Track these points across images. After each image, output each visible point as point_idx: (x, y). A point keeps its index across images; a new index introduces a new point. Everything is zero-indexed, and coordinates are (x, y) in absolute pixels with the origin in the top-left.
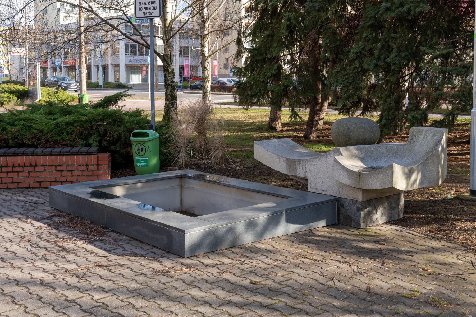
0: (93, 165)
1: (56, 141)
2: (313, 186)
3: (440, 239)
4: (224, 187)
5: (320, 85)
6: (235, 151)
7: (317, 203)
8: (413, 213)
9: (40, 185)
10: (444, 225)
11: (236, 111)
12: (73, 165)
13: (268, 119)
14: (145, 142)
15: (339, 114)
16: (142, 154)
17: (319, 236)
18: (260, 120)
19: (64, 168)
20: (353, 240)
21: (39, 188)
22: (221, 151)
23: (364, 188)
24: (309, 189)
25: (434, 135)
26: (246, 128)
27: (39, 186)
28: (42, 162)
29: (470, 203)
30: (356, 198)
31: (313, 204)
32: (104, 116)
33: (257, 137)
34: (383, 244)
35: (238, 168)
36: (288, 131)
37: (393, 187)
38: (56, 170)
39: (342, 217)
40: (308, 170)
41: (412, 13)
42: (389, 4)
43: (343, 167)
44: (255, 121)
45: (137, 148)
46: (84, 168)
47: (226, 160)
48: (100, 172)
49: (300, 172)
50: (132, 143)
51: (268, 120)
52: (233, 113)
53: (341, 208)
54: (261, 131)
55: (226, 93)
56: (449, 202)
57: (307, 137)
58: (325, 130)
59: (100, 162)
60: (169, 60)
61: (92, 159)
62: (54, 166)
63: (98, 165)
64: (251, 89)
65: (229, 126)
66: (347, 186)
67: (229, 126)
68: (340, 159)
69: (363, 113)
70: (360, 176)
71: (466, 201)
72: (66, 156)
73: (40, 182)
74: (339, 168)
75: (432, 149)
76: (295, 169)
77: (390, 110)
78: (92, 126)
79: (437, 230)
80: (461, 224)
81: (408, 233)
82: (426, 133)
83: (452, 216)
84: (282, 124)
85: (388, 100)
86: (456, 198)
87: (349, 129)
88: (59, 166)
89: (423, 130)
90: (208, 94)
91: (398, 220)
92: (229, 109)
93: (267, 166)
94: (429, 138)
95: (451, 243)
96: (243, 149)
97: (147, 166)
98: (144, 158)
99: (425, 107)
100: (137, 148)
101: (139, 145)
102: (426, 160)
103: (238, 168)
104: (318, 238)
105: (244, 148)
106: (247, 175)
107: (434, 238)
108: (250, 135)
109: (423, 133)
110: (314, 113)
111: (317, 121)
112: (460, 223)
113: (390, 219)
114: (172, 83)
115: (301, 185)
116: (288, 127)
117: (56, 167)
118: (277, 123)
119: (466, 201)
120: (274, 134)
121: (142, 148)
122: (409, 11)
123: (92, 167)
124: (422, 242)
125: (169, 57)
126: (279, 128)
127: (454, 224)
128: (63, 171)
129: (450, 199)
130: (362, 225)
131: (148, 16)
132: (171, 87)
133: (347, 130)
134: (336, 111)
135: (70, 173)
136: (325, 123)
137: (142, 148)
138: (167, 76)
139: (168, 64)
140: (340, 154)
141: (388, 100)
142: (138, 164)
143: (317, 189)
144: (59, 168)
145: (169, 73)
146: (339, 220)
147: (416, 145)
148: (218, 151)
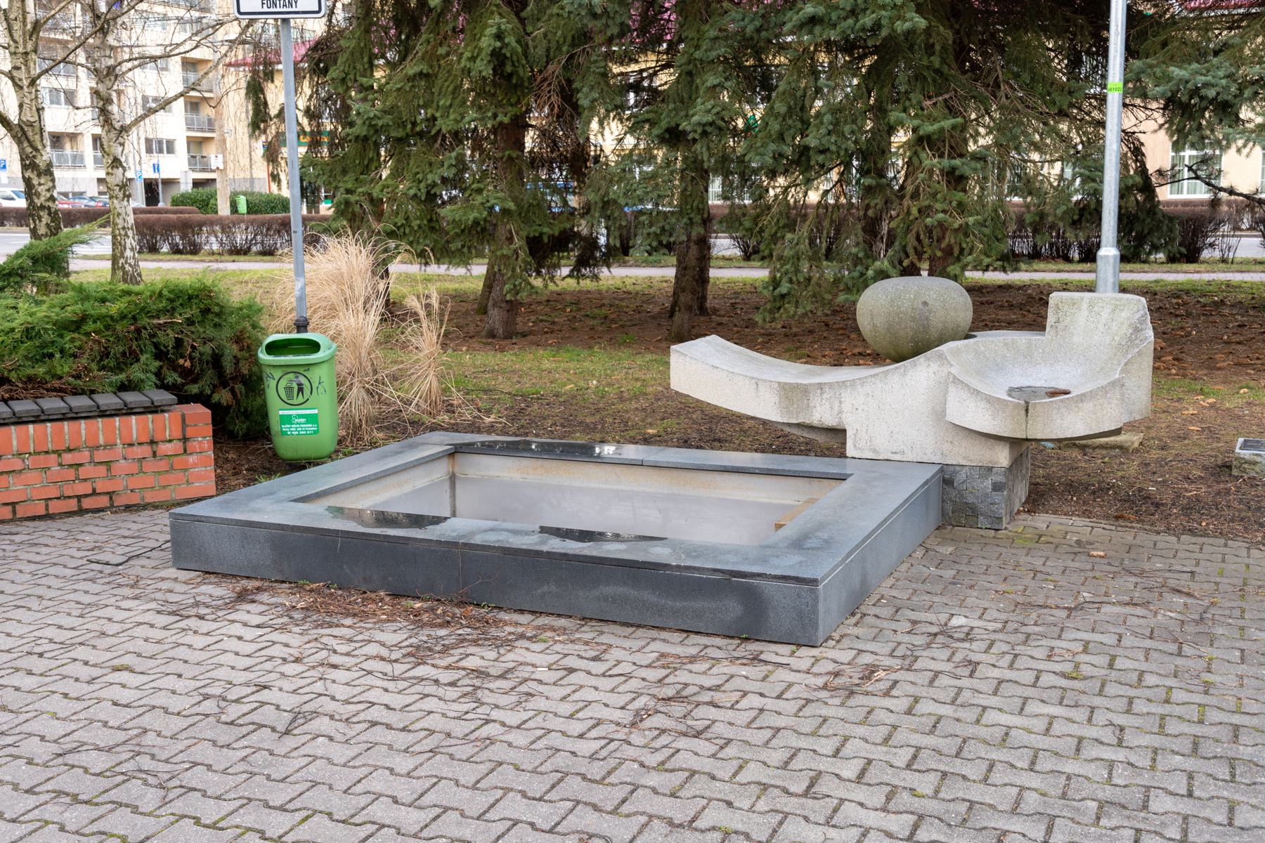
0: (170, 441)
1: (30, 379)
4: (609, 468)
9: (14, 512)
12: (110, 446)
14: (308, 366)
16: (301, 399)
19: (84, 457)
21: (12, 520)
24: (850, 451)
27: (10, 516)
28: (15, 443)
32: (171, 301)
38: (60, 465)
40: (847, 406)
41: (884, 33)
42: (821, 10)
45: (283, 383)
46: (146, 451)
48: (192, 459)
49: (822, 413)
50: (268, 371)
59: (190, 432)
60: (37, 137)
61: (168, 423)
62: (54, 452)
63: (185, 439)
69: (576, 273)
70: (1027, 410)
72: (89, 421)
73: (13, 504)
78: (138, 331)
87: (925, 303)
88: (69, 450)
97: (315, 432)
98: (308, 412)
100: (283, 383)
101: (291, 376)
109: (1085, 306)
114: (50, 204)
117: (60, 455)
121: (300, 385)
122: (877, 26)
123: (169, 445)
125: (37, 130)
128: (81, 465)
131: (278, 10)
132: (49, 214)
135: (103, 469)
137: (300, 385)
138: (35, 182)
139: (37, 150)
142: (285, 428)
143: (874, 451)
144: (68, 458)
145: (39, 175)
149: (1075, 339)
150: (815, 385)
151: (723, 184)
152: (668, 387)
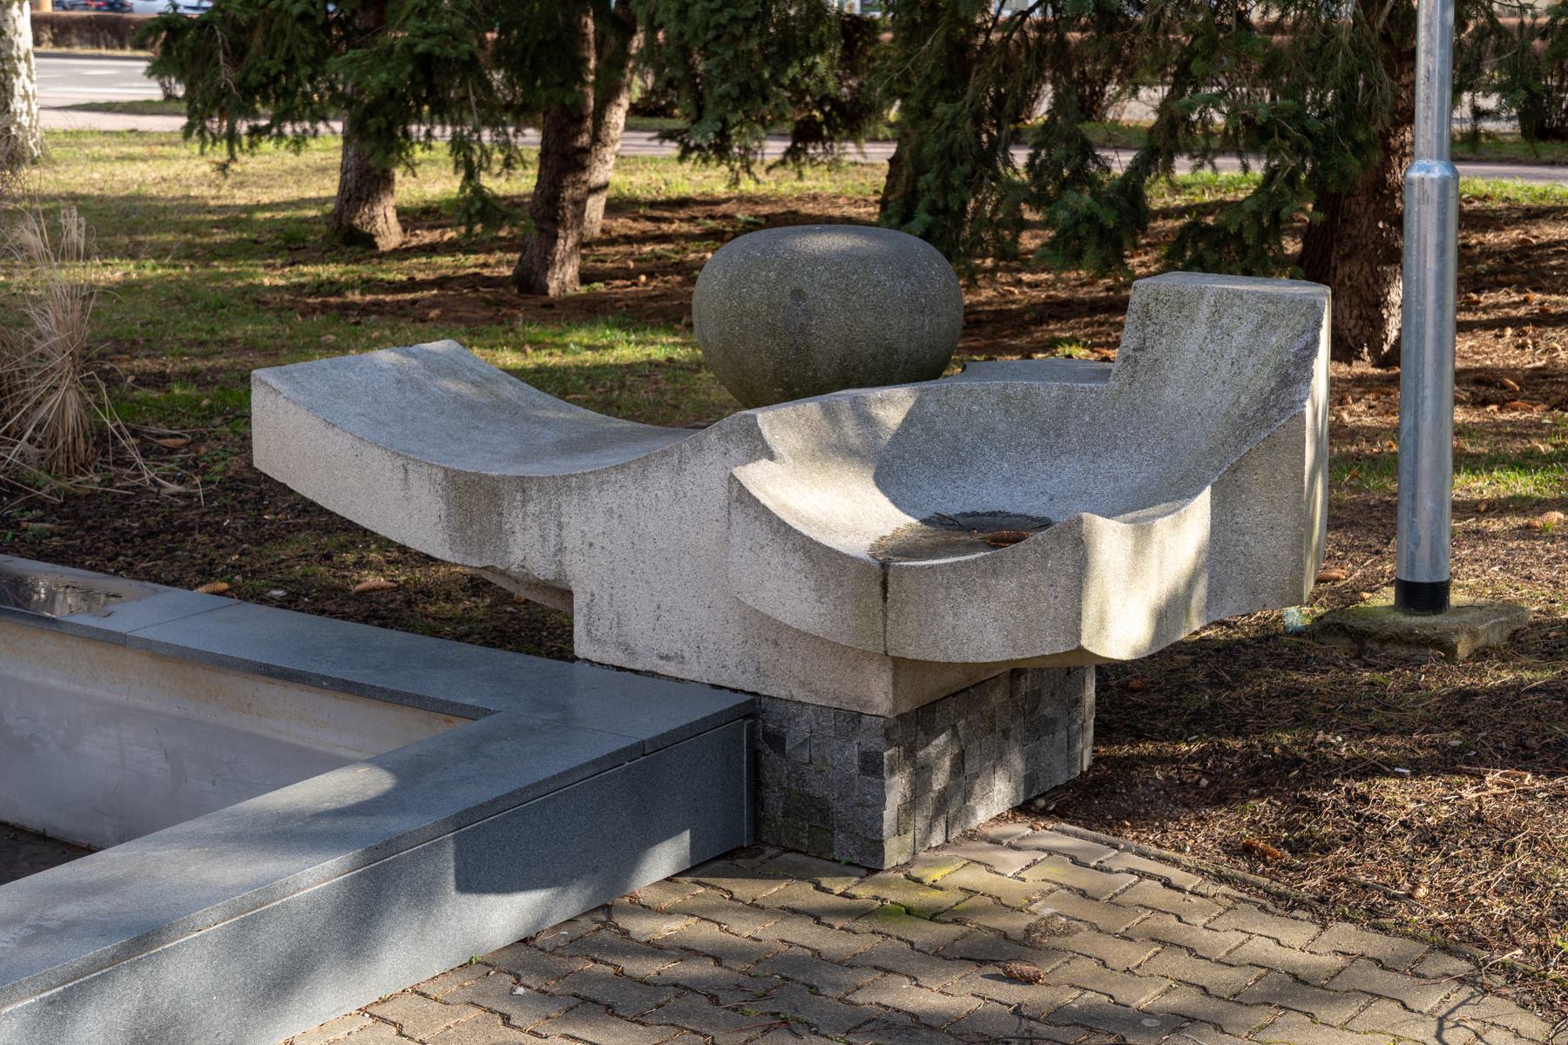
2: (602, 629)
3: (1321, 909)
5: (590, 22)
6: (160, 380)
7: (639, 749)
8: (1139, 737)
10: (1315, 808)
11: (167, 150)
13: (329, 187)
15: (682, 159)
17: (656, 949)
18: (291, 192)
20: (850, 963)
22: (72, 397)
23: (911, 653)
24: (582, 647)
25: (1265, 323)
26: (219, 236)
29: (1404, 652)
30: (855, 700)
31: (616, 758)
33: (277, 288)
34: (1028, 981)
35: (174, 488)
36: (432, 249)
37: (1081, 650)
39: (774, 802)
40: (572, 538)
43: (782, 530)
44: (265, 199)
47: (101, 439)
49: (525, 550)
51: (334, 192)
52: (154, 157)
53: (769, 756)
54: (299, 256)
55: (128, 52)
56: (1298, 651)
57: (529, 282)
58: (612, 242)
64: (238, 53)
65: (131, 231)
66: (801, 635)
67: (131, 231)
68: (763, 480)
71: (1383, 641)
74: (763, 534)
75: (1265, 406)
76: (499, 535)
77: (953, 161)
79: (1286, 844)
80: (1401, 797)
81: (1143, 875)
82: (1217, 312)
83: (1342, 746)
84: (402, 213)
85: (941, 109)
86: (1324, 629)
87: (798, 294)
89: (1202, 294)
90: (22, 67)
91: (1065, 787)
92: (132, 138)
93: (331, 514)
94: (1239, 339)
95: (1382, 929)
96: (201, 365)
99: (1041, 121)
102: (1234, 470)
103: (174, 488)
104: (649, 968)
105: (207, 357)
106: (220, 530)
107: (1288, 905)
108: (238, 276)
109: (1204, 312)
110: (565, 160)
111: (580, 204)
112: (1391, 789)
113: (1028, 790)
115: (528, 623)
116: (431, 228)
118: (379, 210)
119: (1383, 641)
120: (364, 270)
124: (1227, 939)
126: (389, 233)
127: (1364, 799)
129: (1298, 633)
130: (894, 851)
133: (788, 301)
134: (667, 143)
136: (615, 207)
140: (761, 450)
141: (941, 109)
143: (627, 648)
146: (757, 821)
147: (1165, 380)
148: (55, 399)
149: (1169, 395)
150: (510, 480)
151: (1163, 108)
152: (250, 465)
